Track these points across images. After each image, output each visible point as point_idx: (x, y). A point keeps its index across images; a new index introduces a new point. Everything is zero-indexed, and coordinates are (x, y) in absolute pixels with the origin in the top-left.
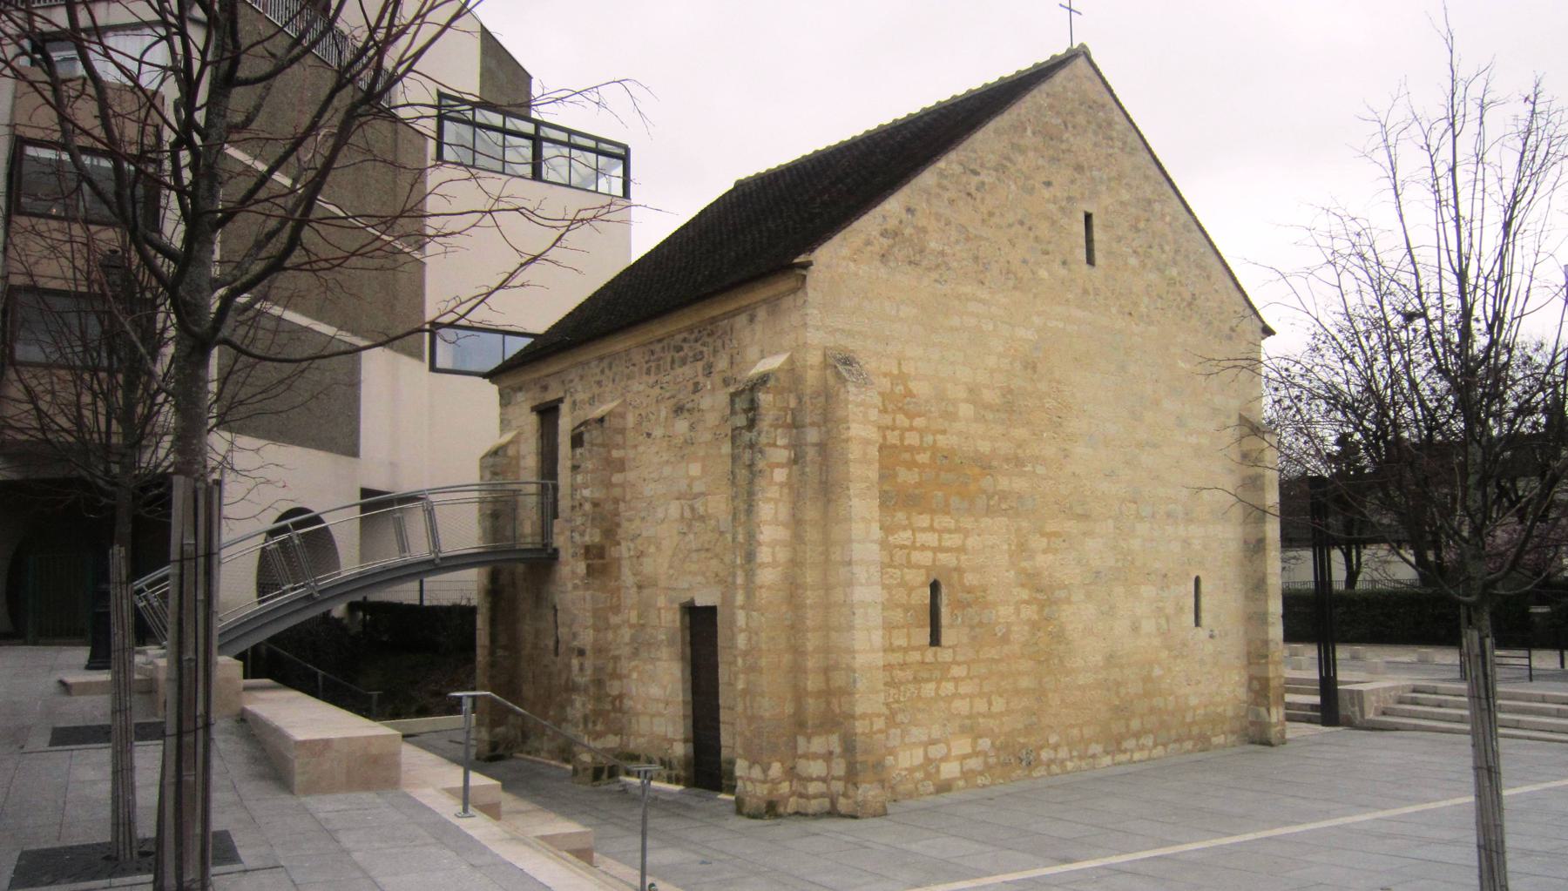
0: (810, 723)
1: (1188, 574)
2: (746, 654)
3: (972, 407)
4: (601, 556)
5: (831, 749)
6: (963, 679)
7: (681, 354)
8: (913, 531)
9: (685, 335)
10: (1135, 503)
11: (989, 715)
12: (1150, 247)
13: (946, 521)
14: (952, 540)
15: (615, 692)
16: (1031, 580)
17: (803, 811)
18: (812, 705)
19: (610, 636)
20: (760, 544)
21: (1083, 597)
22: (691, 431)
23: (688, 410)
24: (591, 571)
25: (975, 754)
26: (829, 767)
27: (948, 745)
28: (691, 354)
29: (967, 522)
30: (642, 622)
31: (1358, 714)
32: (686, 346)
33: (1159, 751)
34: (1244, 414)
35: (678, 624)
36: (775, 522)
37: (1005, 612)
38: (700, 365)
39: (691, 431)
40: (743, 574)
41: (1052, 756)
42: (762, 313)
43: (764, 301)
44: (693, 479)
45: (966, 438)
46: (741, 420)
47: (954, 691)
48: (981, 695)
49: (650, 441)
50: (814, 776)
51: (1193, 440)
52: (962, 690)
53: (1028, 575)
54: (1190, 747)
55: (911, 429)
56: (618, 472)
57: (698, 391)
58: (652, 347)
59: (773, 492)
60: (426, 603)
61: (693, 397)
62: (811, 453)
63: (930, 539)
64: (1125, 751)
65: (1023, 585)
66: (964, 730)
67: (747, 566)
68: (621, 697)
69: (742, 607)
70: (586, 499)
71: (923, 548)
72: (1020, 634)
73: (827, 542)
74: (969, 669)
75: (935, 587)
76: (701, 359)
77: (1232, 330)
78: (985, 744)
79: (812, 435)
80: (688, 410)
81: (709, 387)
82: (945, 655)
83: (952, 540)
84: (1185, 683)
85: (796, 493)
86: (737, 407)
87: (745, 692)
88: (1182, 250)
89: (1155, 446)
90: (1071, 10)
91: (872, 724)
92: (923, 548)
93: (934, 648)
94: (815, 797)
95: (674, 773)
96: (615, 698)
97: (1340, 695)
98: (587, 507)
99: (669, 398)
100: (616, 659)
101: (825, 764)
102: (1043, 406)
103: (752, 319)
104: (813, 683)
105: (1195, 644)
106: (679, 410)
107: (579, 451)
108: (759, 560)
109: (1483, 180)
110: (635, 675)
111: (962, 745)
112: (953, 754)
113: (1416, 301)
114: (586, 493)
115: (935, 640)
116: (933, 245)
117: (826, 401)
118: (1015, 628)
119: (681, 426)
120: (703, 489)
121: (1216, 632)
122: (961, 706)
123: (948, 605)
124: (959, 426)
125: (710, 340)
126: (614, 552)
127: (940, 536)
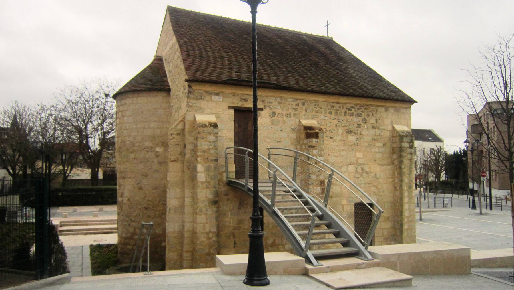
2: (408, 217)
9: (353, 105)
20: (198, 172)
21: (208, 180)
22: (356, 141)
39: (356, 141)
40: (408, 192)
42: (392, 110)
43: (395, 107)
44: (358, 158)
49: (332, 140)
58: (334, 104)
61: (357, 129)
67: (409, 190)
76: (361, 116)
87: (407, 229)
90: (327, 25)
103: (387, 110)
119: (352, 138)
120: (363, 162)
125: (366, 111)
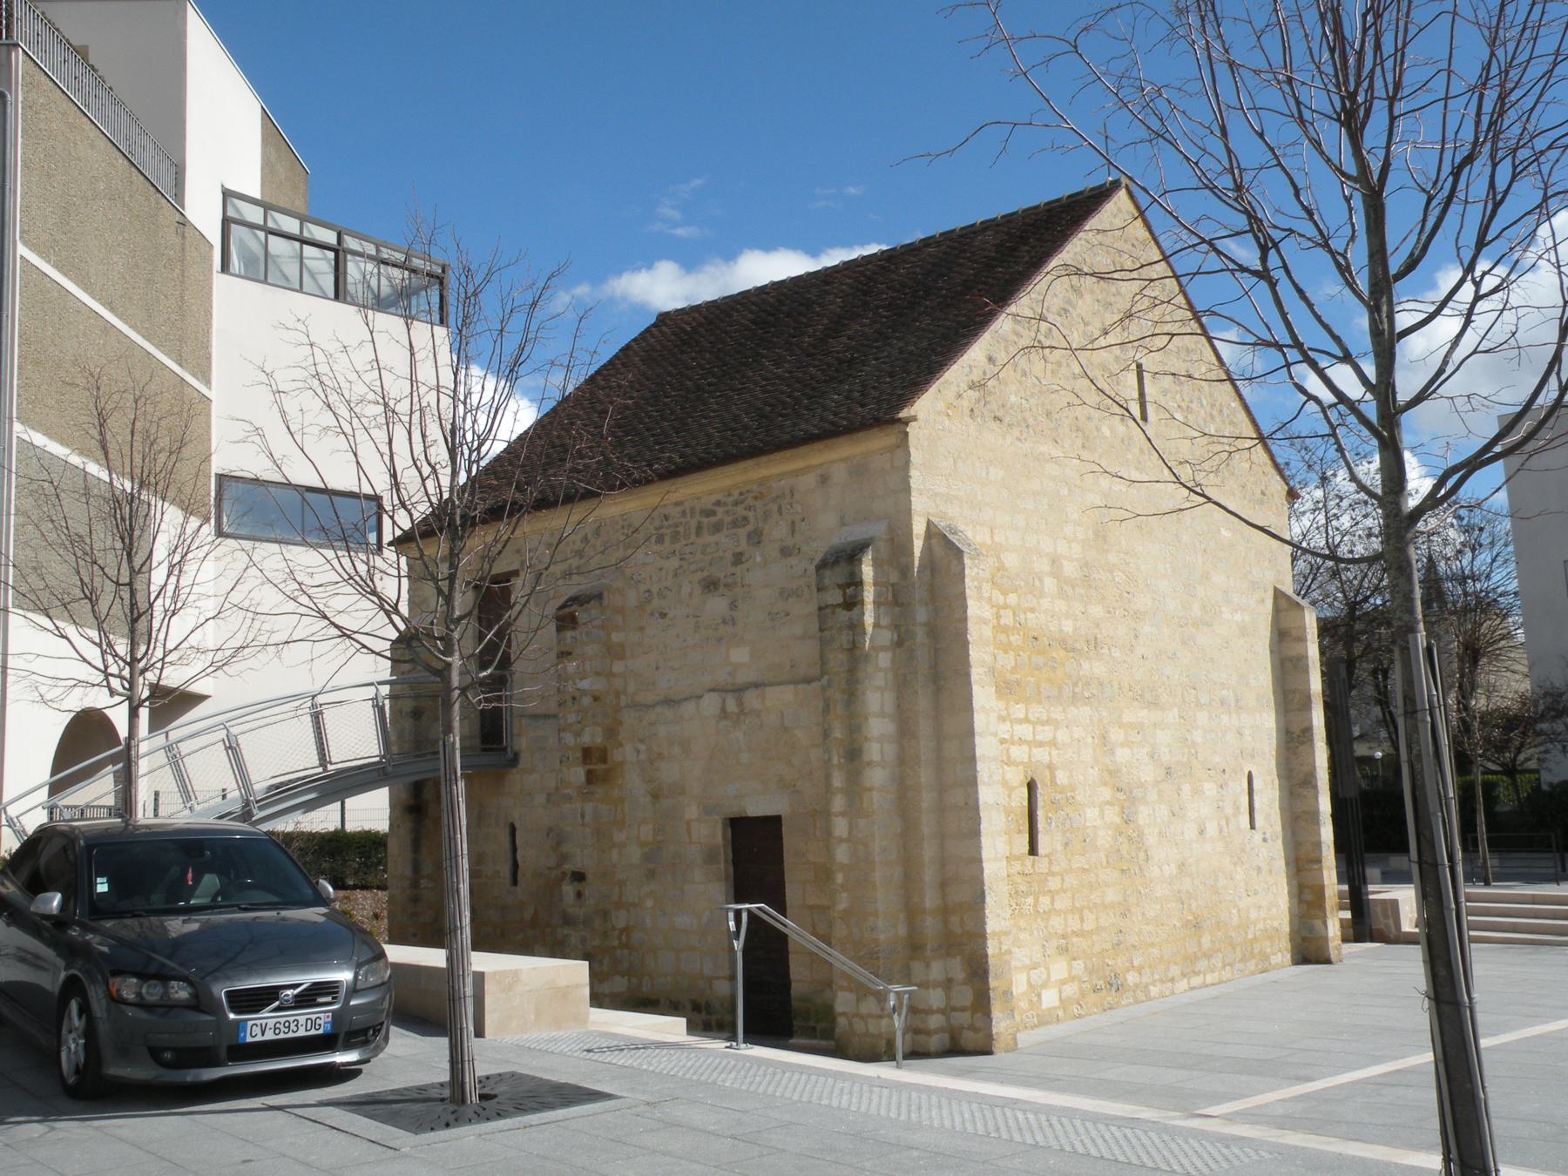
0: (929, 947)
1: (1242, 770)
3: (1055, 581)
4: (604, 760)
5: (950, 976)
6: (1058, 892)
7: (713, 519)
8: (1011, 722)
10: (1194, 689)
11: (1081, 934)
12: (1191, 402)
13: (1037, 711)
14: (1045, 733)
15: (621, 924)
16: (1112, 775)
17: (921, 1050)
18: (930, 925)
19: (615, 854)
23: (725, 585)
24: (591, 777)
25: (1072, 979)
26: (948, 997)
27: (1047, 969)
28: (728, 519)
29: (1057, 714)
30: (659, 838)
31: (1393, 927)
32: (720, 510)
33: (1227, 974)
34: (1278, 586)
35: (719, 839)
36: (882, 714)
37: (1091, 814)
38: (742, 532)
39: (731, 609)
41: (1138, 980)
45: (1052, 617)
46: (835, 597)
47: (1051, 907)
48: (1073, 910)
50: (935, 1008)
51: (1238, 617)
52: (1058, 905)
53: (1110, 773)
54: (1253, 968)
55: (1006, 606)
56: (619, 659)
57: (742, 563)
59: (879, 680)
60: (349, 827)
62: (920, 635)
63: (1024, 731)
64: (1198, 973)
65: (1105, 784)
66: (1063, 950)
68: (626, 930)
69: (843, 814)
70: (583, 692)
71: (1021, 741)
72: (1104, 839)
73: (939, 737)
74: (1063, 880)
75: (1031, 787)
77: (1263, 493)
78: (1079, 966)
79: (921, 615)
80: (725, 585)
81: (758, 559)
82: (1041, 864)
83: (1045, 733)
84: (1245, 895)
85: (902, 684)
86: (827, 582)
88: (1218, 404)
89: (1209, 625)
91: (1000, 943)
92: (1021, 741)
93: (1031, 857)
94: (937, 1031)
95: (714, 1018)
96: (622, 931)
97: (1371, 904)
98: (586, 701)
99: (694, 572)
100: (622, 883)
101: (943, 993)
102: (1114, 580)
104: (930, 900)
105: (1252, 849)
106: (711, 585)
107: (569, 634)
108: (866, 758)
109: (1285, 267)
110: (649, 903)
111: (1059, 969)
112: (1053, 979)
113: (382, 271)
114: (584, 684)
115: (1033, 850)
116: (1013, 399)
117: (932, 575)
118: (1101, 833)
119: (717, 605)
121: (1268, 836)
122: (1057, 923)
123: (1044, 807)
124: (1045, 603)
126: (616, 755)
127: (1034, 728)
